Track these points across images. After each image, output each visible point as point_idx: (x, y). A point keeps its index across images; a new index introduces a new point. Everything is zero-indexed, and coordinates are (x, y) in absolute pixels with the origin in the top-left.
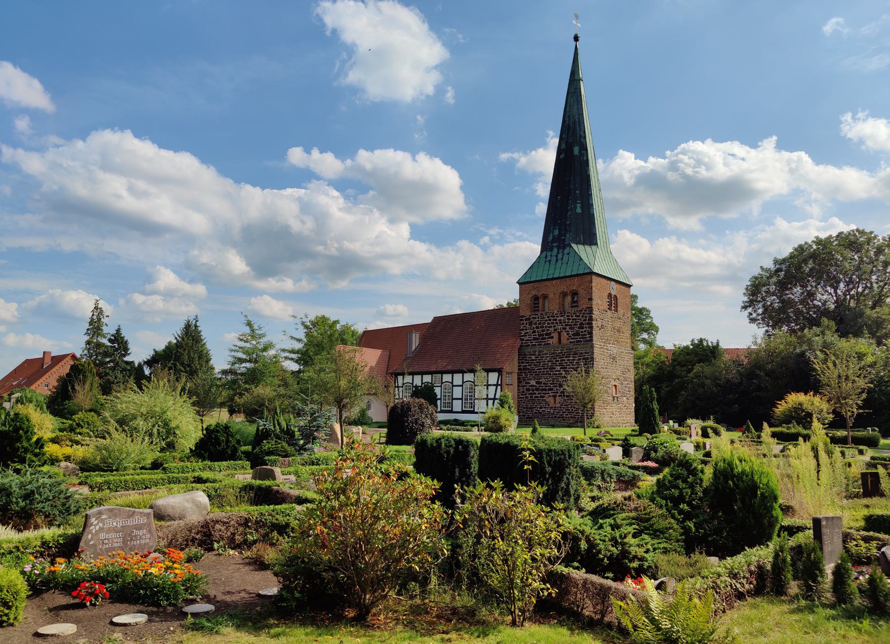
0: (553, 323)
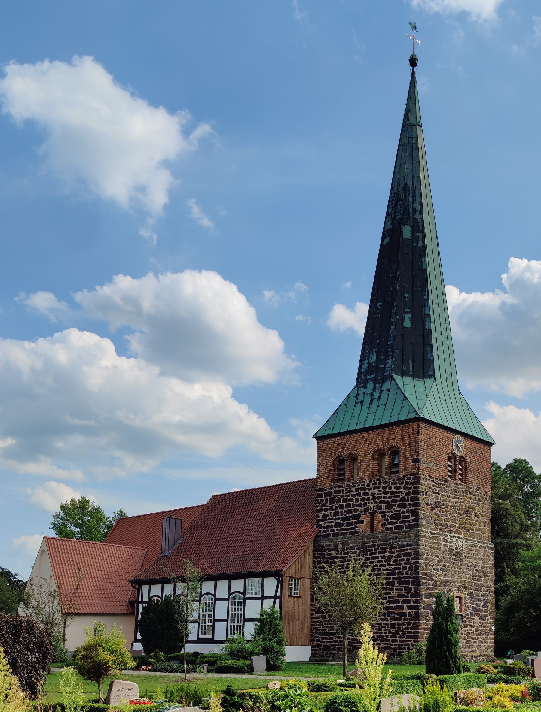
0: (363, 500)
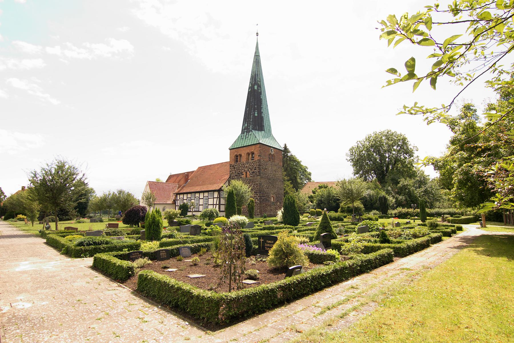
0: (243, 168)
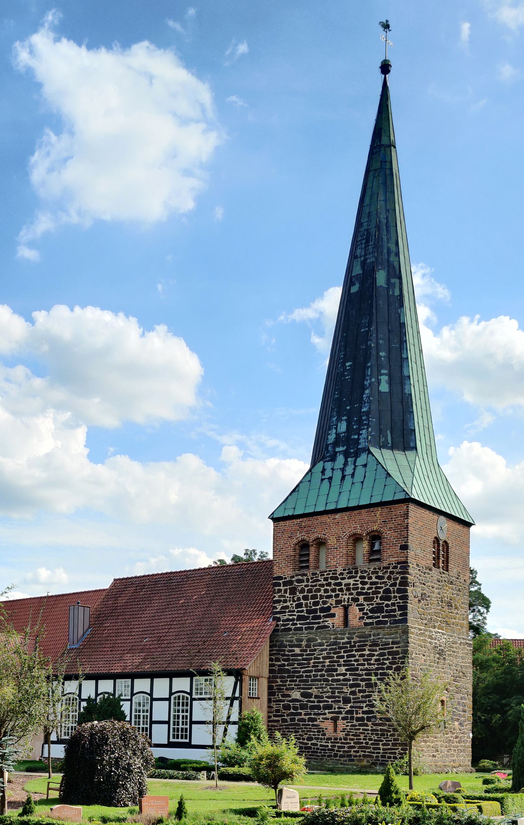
0: (334, 590)
